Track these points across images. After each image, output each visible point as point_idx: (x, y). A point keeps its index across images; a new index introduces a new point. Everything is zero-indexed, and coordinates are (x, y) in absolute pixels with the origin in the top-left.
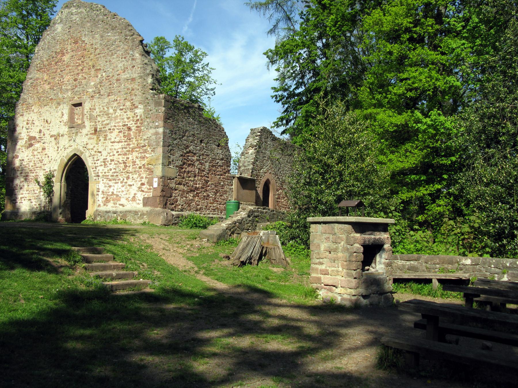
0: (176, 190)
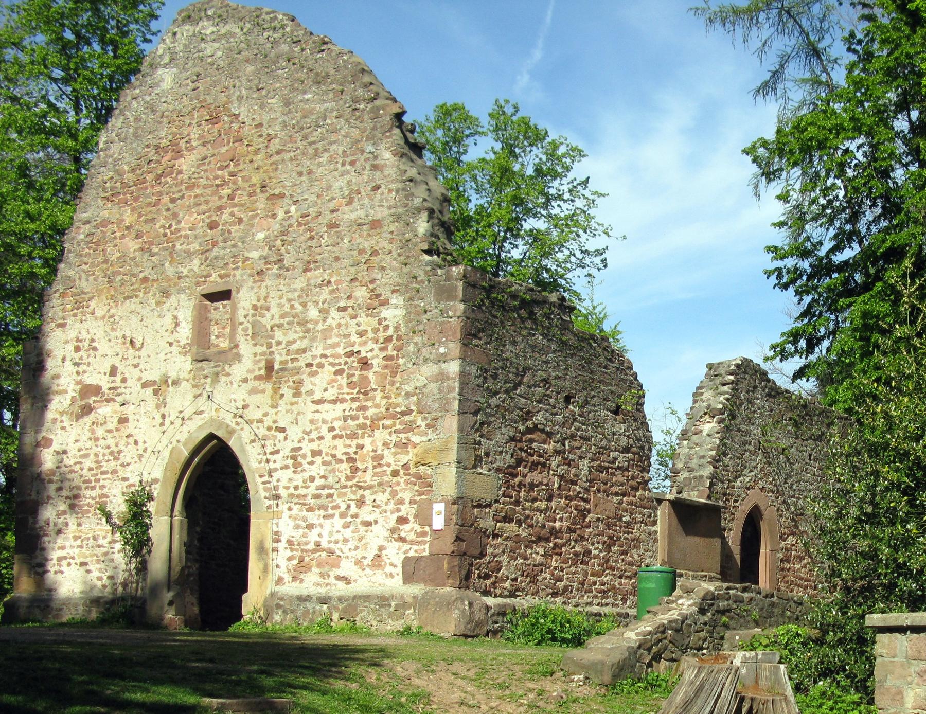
0: (496, 536)
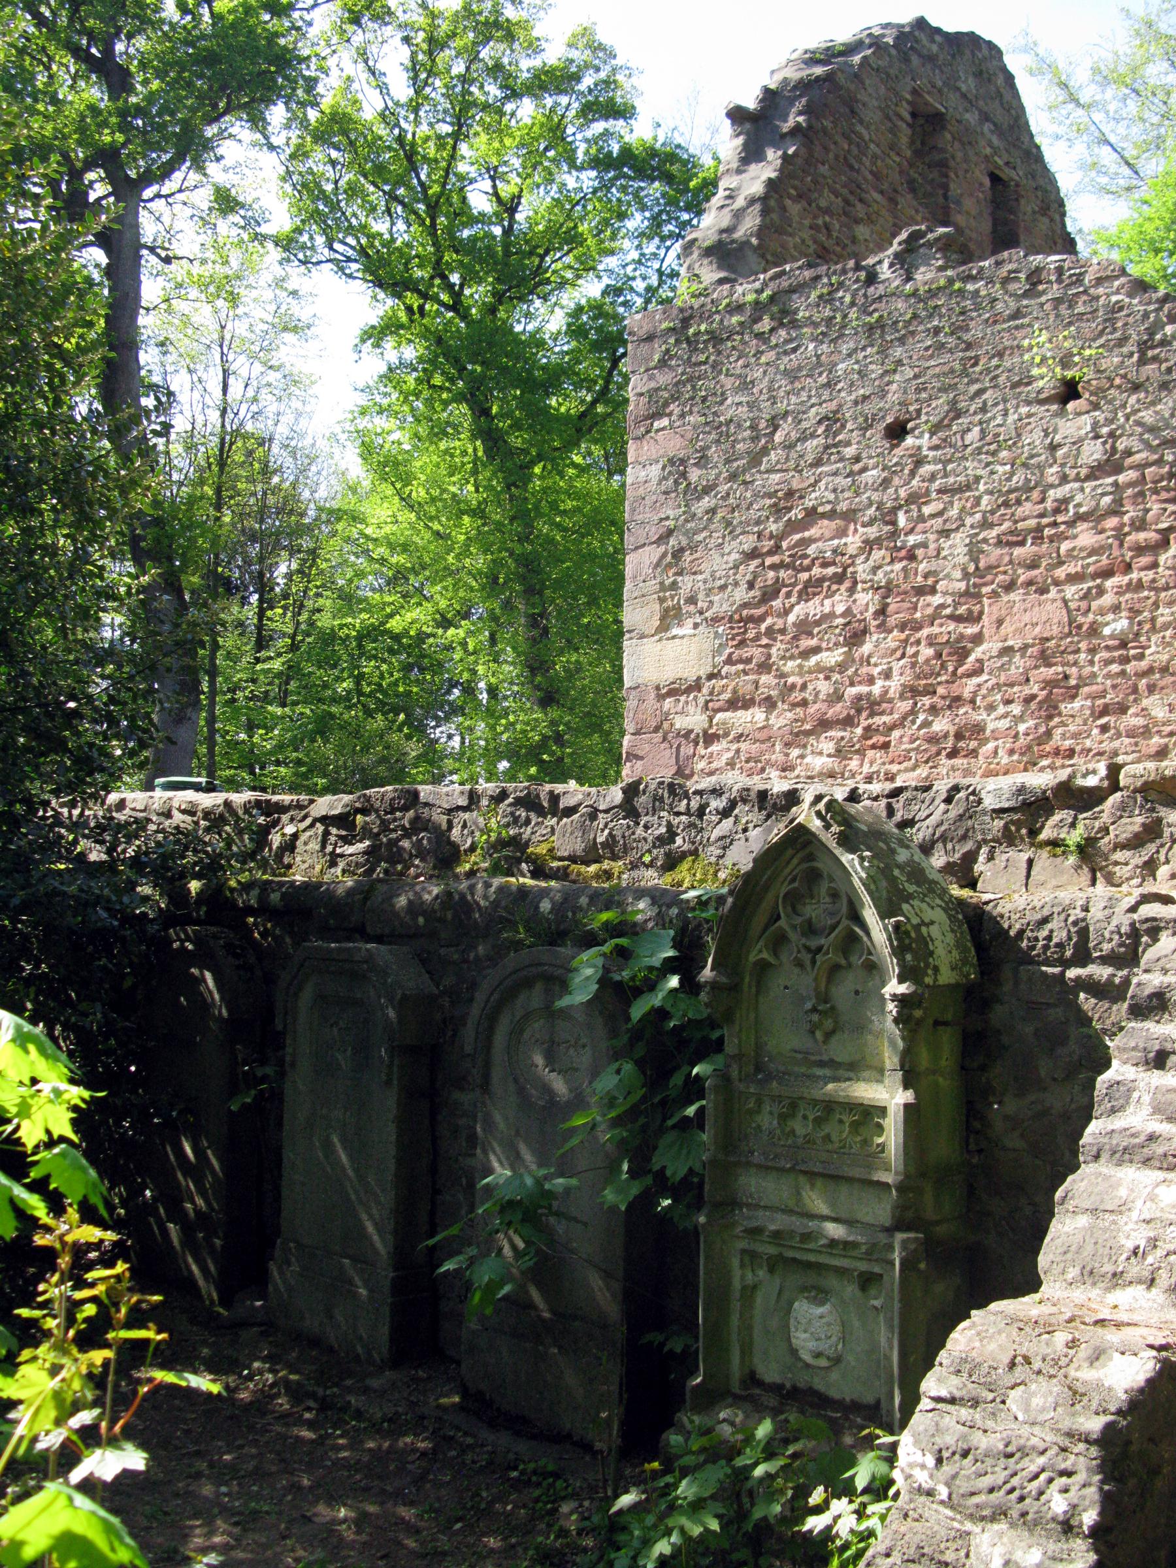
0: (710, 738)
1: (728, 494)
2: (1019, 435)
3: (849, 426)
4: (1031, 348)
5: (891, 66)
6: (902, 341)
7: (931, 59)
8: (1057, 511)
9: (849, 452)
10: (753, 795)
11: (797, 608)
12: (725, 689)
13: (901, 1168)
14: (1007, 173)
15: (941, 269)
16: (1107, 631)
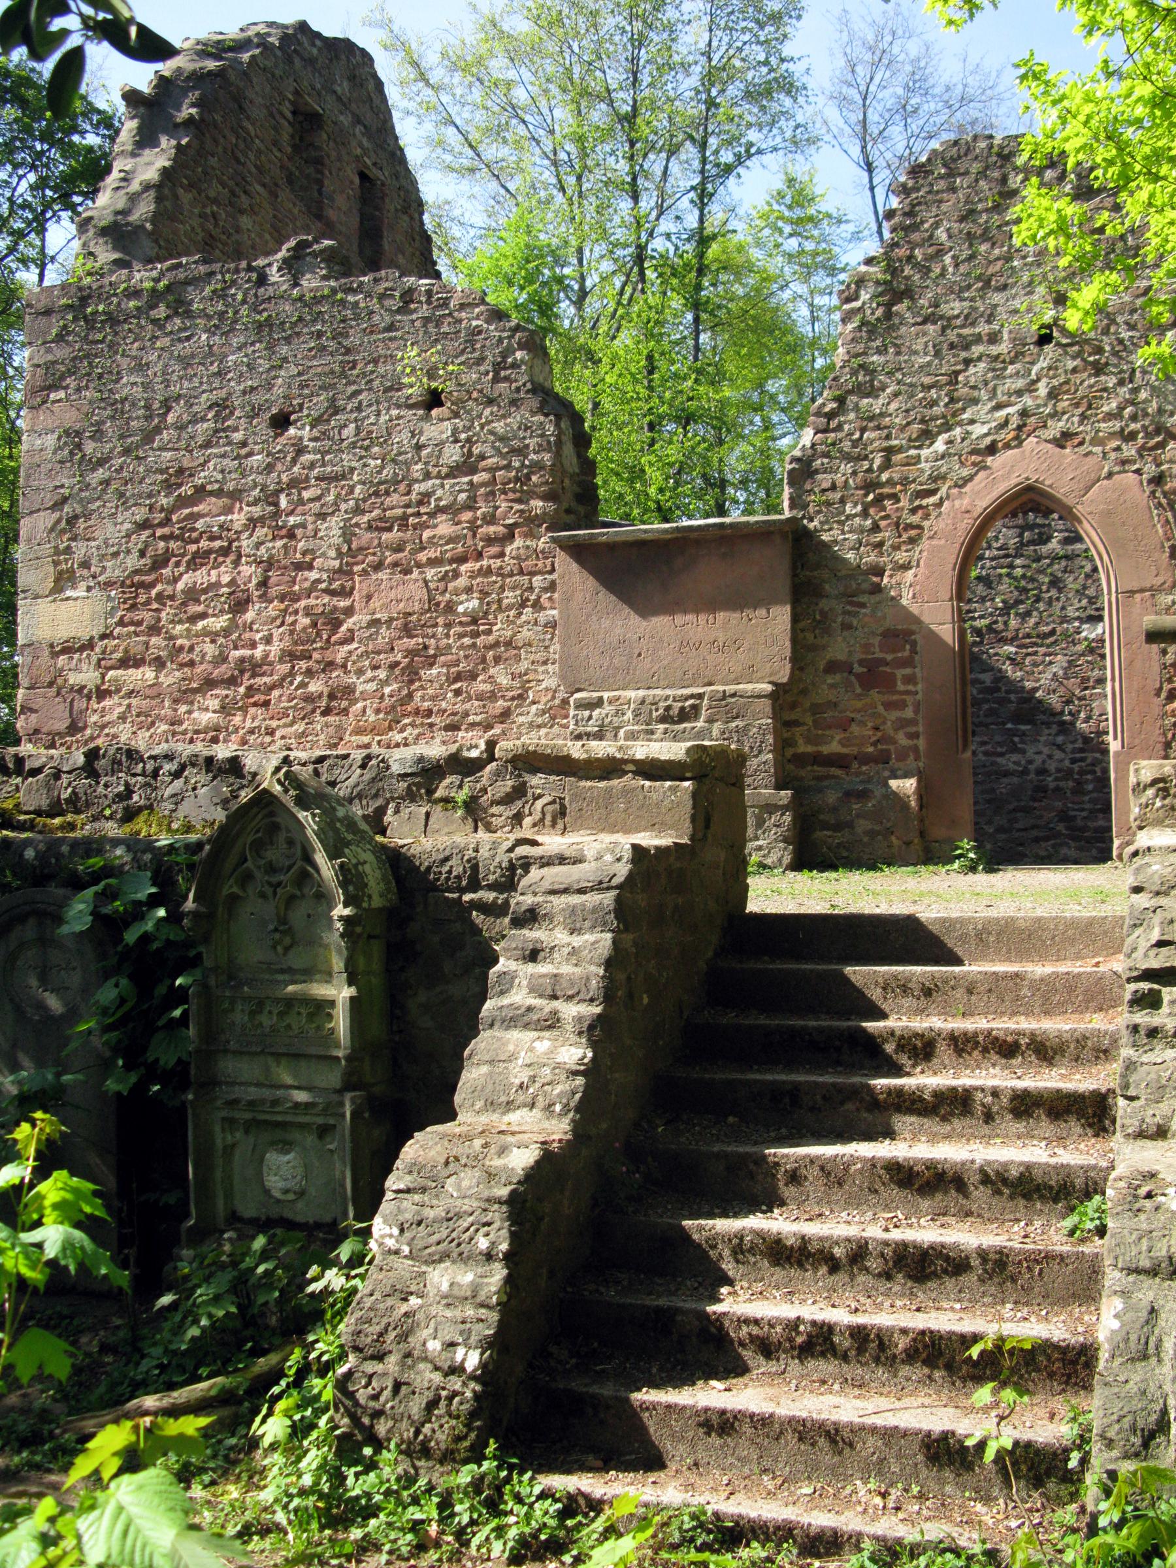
0: (102, 694)
1: (122, 468)
2: (389, 434)
3: (237, 413)
4: (402, 358)
5: (276, 66)
6: (288, 340)
7: (310, 61)
8: (420, 503)
9: (238, 436)
10: (201, 760)
11: (185, 577)
12: (117, 648)
13: (349, 1044)
14: (374, 173)
15: (325, 278)
16: (461, 609)
